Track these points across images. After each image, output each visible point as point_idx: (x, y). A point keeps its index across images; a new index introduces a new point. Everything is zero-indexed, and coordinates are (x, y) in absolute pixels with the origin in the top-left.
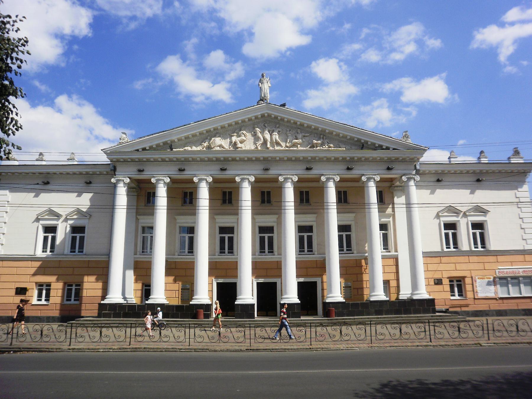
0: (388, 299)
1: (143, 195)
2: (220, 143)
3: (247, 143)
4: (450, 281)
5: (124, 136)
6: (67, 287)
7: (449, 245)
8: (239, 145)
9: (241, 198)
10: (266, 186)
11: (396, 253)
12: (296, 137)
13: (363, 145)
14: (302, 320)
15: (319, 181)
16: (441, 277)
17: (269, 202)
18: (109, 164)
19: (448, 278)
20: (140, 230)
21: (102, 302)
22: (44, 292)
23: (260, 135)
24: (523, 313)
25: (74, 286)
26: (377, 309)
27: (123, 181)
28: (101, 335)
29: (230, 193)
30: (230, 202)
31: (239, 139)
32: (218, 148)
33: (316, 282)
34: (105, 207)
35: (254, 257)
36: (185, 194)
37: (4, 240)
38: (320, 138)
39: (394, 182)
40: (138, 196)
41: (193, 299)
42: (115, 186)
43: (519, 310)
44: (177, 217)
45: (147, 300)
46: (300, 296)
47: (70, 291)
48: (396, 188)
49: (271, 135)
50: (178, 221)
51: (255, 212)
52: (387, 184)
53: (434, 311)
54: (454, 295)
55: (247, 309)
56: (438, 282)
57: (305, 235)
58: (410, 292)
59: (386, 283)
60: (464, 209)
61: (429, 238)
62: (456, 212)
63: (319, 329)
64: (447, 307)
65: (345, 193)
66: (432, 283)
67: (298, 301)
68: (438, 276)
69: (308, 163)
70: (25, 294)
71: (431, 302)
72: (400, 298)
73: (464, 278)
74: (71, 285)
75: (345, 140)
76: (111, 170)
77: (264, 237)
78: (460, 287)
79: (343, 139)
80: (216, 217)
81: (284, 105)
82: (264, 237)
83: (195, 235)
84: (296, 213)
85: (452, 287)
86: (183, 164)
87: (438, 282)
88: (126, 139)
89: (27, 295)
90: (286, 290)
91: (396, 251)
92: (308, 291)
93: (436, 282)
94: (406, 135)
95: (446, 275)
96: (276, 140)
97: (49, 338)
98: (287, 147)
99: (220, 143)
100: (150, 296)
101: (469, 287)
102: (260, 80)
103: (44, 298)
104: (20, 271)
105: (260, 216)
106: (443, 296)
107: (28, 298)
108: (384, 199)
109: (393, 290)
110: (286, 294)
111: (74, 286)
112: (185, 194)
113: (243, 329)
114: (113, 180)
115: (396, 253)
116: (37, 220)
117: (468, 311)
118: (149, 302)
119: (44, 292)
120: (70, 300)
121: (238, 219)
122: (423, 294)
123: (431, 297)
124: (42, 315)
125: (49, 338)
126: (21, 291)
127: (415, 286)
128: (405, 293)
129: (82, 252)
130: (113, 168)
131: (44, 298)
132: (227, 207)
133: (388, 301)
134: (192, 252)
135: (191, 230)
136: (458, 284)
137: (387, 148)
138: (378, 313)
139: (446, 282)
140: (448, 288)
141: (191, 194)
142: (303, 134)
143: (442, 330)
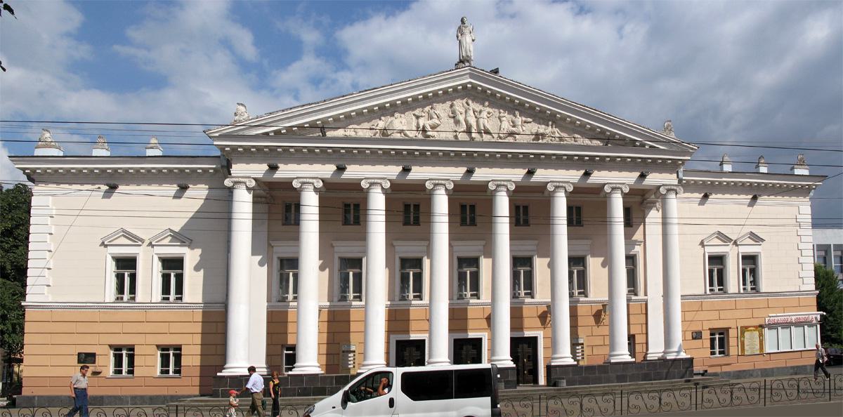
0: (634, 360)
2: (403, 123)
4: (711, 334)
5: (241, 108)
6: (159, 353)
9: (553, 214)
10: (468, 198)
11: (646, 297)
12: (513, 122)
13: (608, 140)
14: (519, 391)
15: (486, 192)
16: (701, 329)
17: (473, 223)
18: (219, 157)
19: (710, 329)
22: (125, 360)
23: (461, 118)
24: (792, 371)
26: (619, 374)
27: (245, 183)
28: (798, 392)
29: (417, 207)
30: (417, 222)
31: (430, 122)
32: (398, 136)
33: (481, 339)
34: (212, 229)
36: (347, 206)
37: (51, 279)
39: (647, 196)
40: (269, 213)
41: (224, 369)
42: (230, 190)
43: (787, 368)
44: (335, 243)
45: (290, 369)
48: (649, 205)
50: (336, 249)
51: (453, 237)
52: (638, 199)
53: (692, 374)
56: (697, 336)
58: (663, 350)
59: (631, 338)
60: (734, 239)
61: (690, 277)
62: (725, 239)
63: (551, 402)
64: (705, 368)
65: (579, 209)
66: (689, 336)
67: (512, 364)
69: (531, 162)
71: (690, 361)
72: (648, 359)
73: (727, 329)
74: (121, 350)
75: (583, 130)
76: (222, 167)
78: (723, 343)
79: (579, 129)
80: (395, 243)
81: (496, 71)
83: (725, 266)
84: (511, 239)
85: (712, 341)
86: (342, 158)
87: (697, 336)
88: (246, 115)
89: (97, 364)
90: (434, 353)
91: (646, 295)
93: (694, 336)
94: (669, 125)
95: (707, 326)
98: (500, 138)
100: (295, 363)
101: (733, 341)
102: (460, 28)
104: (163, 328)
105: (460, 243)
106: (701, 354)
107: (98, 369)
108: (633, 218)
109: (638, 348)
112: (407, 207)
113: (530, 402)
114: (228, 183)
115: (646, 297)
117: (729, 373)
118: (295, 372)
119: (125, 360)
121: (429, 244)
122: (679, 351)
123: (689, 356)
124: (124, 393)
126: (86, 359)
127: (668, 342)
128: (656, 350)
129: (181, 299)
130: (226, 164)
132: (412, 229)
133: (634, 362)
136: (720, 339)
138: (621, 379)
139: (706, 335)
140: (708, 343)
141: (357, 206)
143: (713, 397)
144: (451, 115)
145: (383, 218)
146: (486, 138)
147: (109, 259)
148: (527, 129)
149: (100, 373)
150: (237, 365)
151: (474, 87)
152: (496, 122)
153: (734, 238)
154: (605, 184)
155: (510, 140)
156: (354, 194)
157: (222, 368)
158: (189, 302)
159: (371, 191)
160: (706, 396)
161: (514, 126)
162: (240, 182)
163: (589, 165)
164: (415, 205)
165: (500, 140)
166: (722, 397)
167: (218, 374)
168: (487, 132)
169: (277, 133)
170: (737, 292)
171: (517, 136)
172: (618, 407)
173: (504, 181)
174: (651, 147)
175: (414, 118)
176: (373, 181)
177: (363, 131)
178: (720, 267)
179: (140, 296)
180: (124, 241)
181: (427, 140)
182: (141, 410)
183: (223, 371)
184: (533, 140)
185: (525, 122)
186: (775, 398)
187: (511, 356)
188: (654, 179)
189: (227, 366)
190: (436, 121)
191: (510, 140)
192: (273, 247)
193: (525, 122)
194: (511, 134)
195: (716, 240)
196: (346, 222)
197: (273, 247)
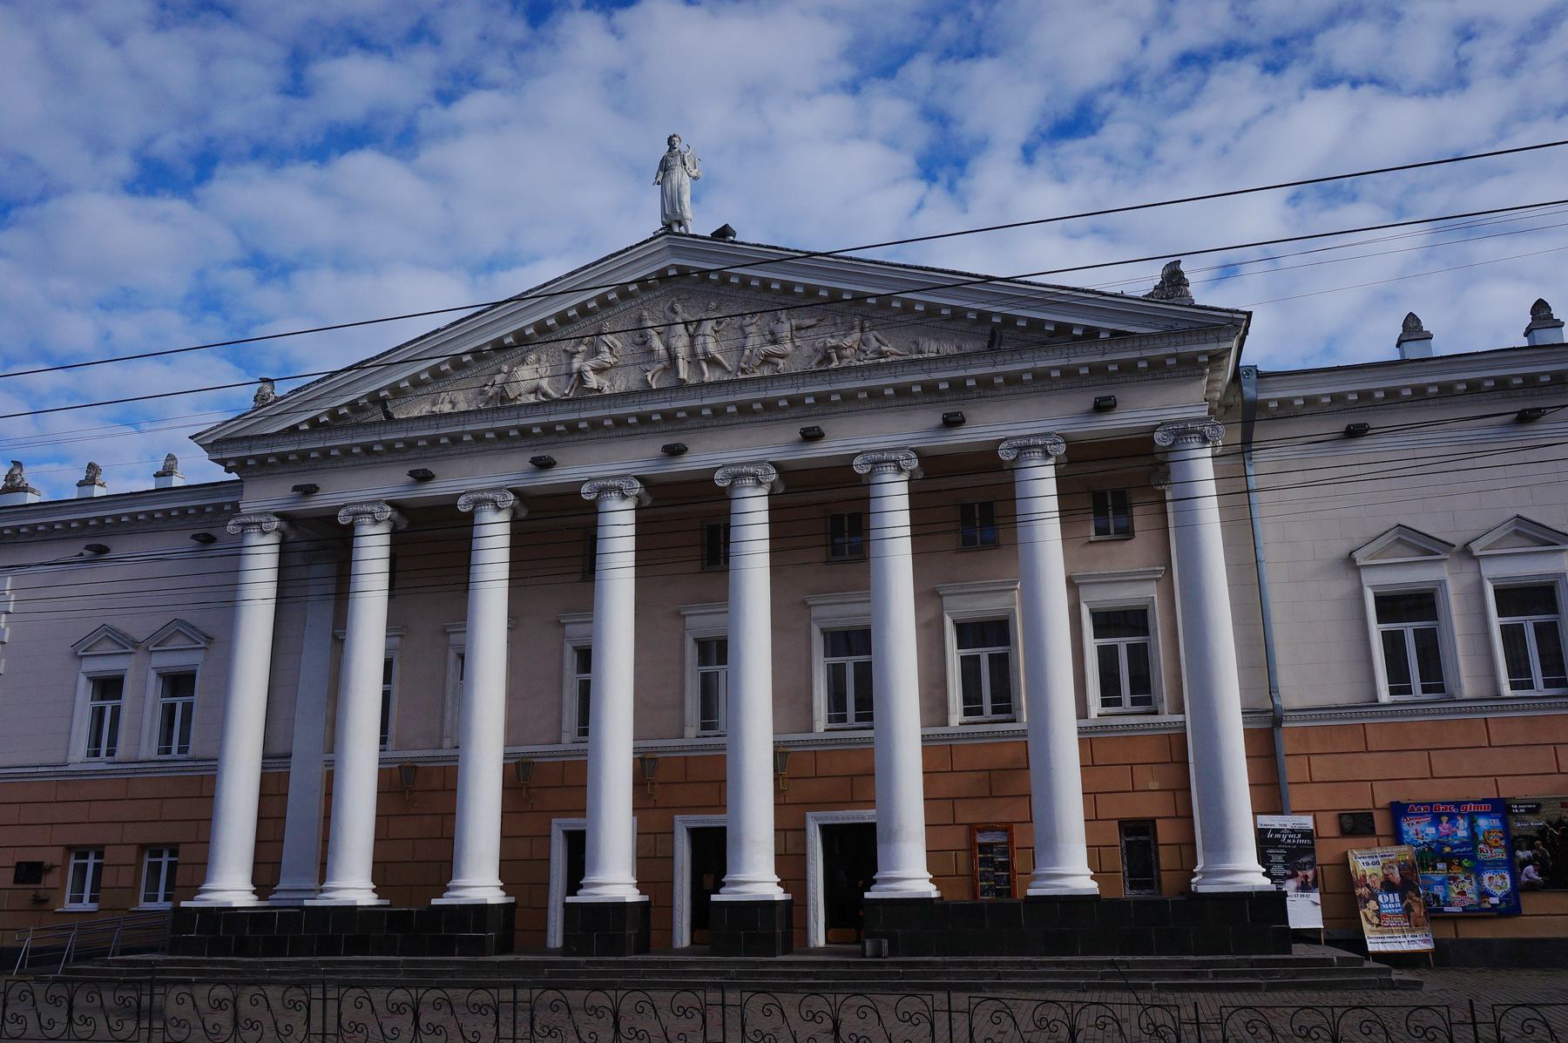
0: (1143, 895)
1: (317, 553)
2: (531, 375)
3: (610, 369)
6: (73, 861)
7: (1117, 689)
8: (593, 381)
11: (1179, 718)
12: (772, 333)
20: (691, 652)
21: (570, 899)
23: (657, 344)
25: (92, 856)
28: (417, 1026)
29: (987, 508)
31: (593, 362)
32: (532, 399)
35: (1084, 723)
38: (853, 328)
46: (507, 885)
47: (155, 869)
49: (692, 337)
50: (816, 612)
54: (80, 900)
55: (768, 926)
57: (850, 662)
62: (1428, 547)
68: (1356, 801)
70: (39, 882)
77: (978, 657)
81: (724, 233)
82: (978, 657)
83: (874, 658)
92: (1134, 845)
93: (1347, 827)
96: (706, 353)
97: (186, 1030)
99: (531, 375)
103: (87, 894)
110: (460, 876)
111: (92, 856)
116: (81, 652)
120: (80, 900)
125: (186, 1030)
126: (29, 872)
131: (87, 894)
134: (870, 718)
135: (586, 658)
137: (1091, 334)
142: (794, 322)
144: (639, 340)
145: (765, 546)
146: (709, 375)
147: (83, 680)
148: (795, 345)
149: (45, 901)
150: (757, 876)
151: (683, 272)
152: (712, 344)
153: (1457, 539)
154: (1154, 428)
155: (767, 371)
156: (992, 478)
157: (442, 887)
158: (20, 763)
159: (737, 494)
160: (349, 1012)
161: (774, 342)
162: (1029, 447)
163: (949, 404)
164: (982, 505)
165: (741, 376)
166: (48, 1012)
167: (434, 902)
168: (713, 362)
169: (314, 422)
170: (1486, 694)
171: (781, 361)
172: (316, 1024)
173: (255, 514)
174: (1115, 333)
175: (563, 356)
176: (878, 456)
177: (458, 398)
178: (862, 658)
179: (122, 751)
180: (108, 647)
181: (583, 395)
182: (1257, 1016)
183: (1034, 884)
184: (820, 363)
185: (799, 328)
186: (1436, 1020)
187: (373, 880)
188: (1140, 411)
189: (455, 882)
190: (607, 358)
191: (767, 371)
192: (941, 597)
193: (799, 328)
194: (767, 359)
195: (1400, 548)
196: (968, 544)
197: (1476, 559)
